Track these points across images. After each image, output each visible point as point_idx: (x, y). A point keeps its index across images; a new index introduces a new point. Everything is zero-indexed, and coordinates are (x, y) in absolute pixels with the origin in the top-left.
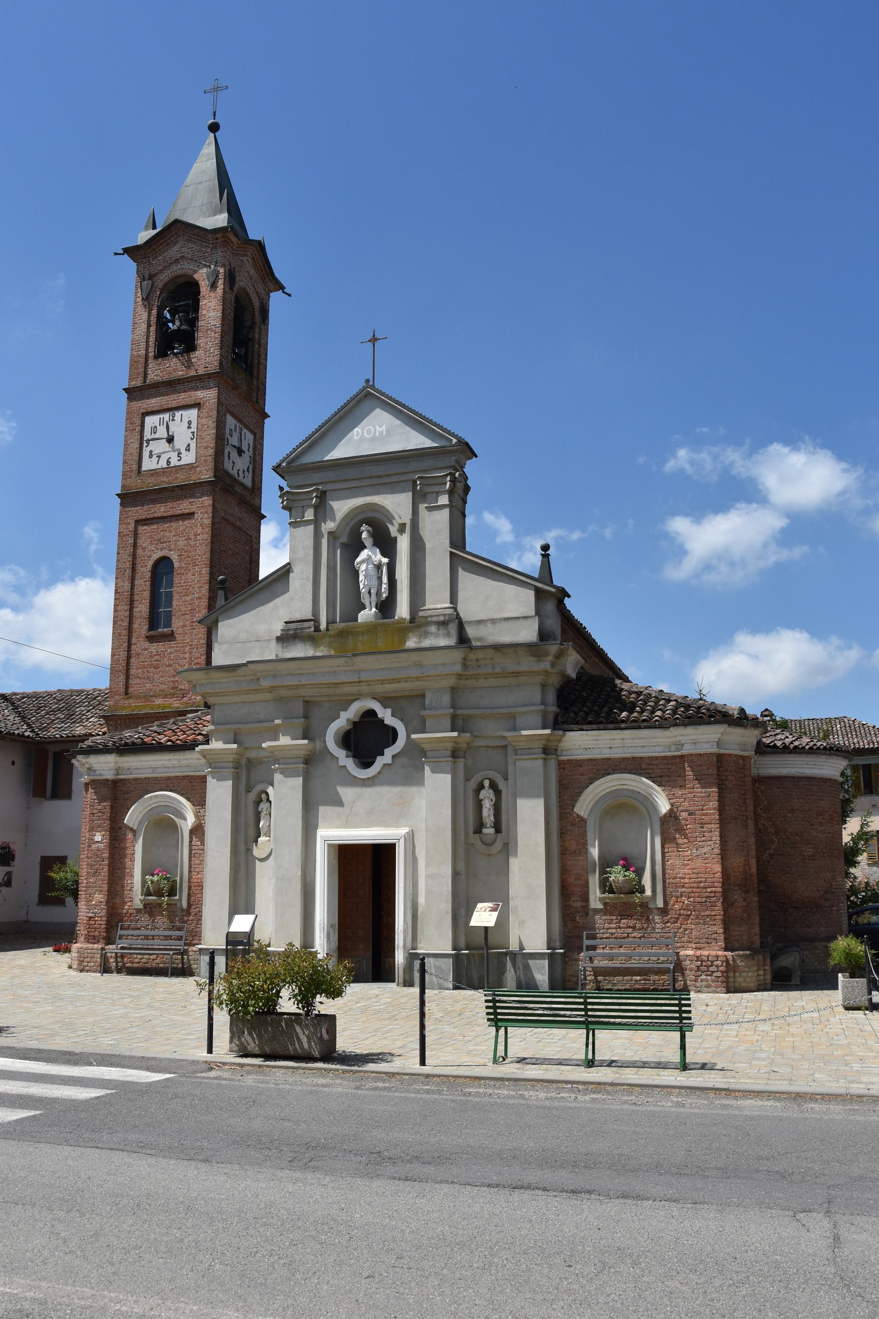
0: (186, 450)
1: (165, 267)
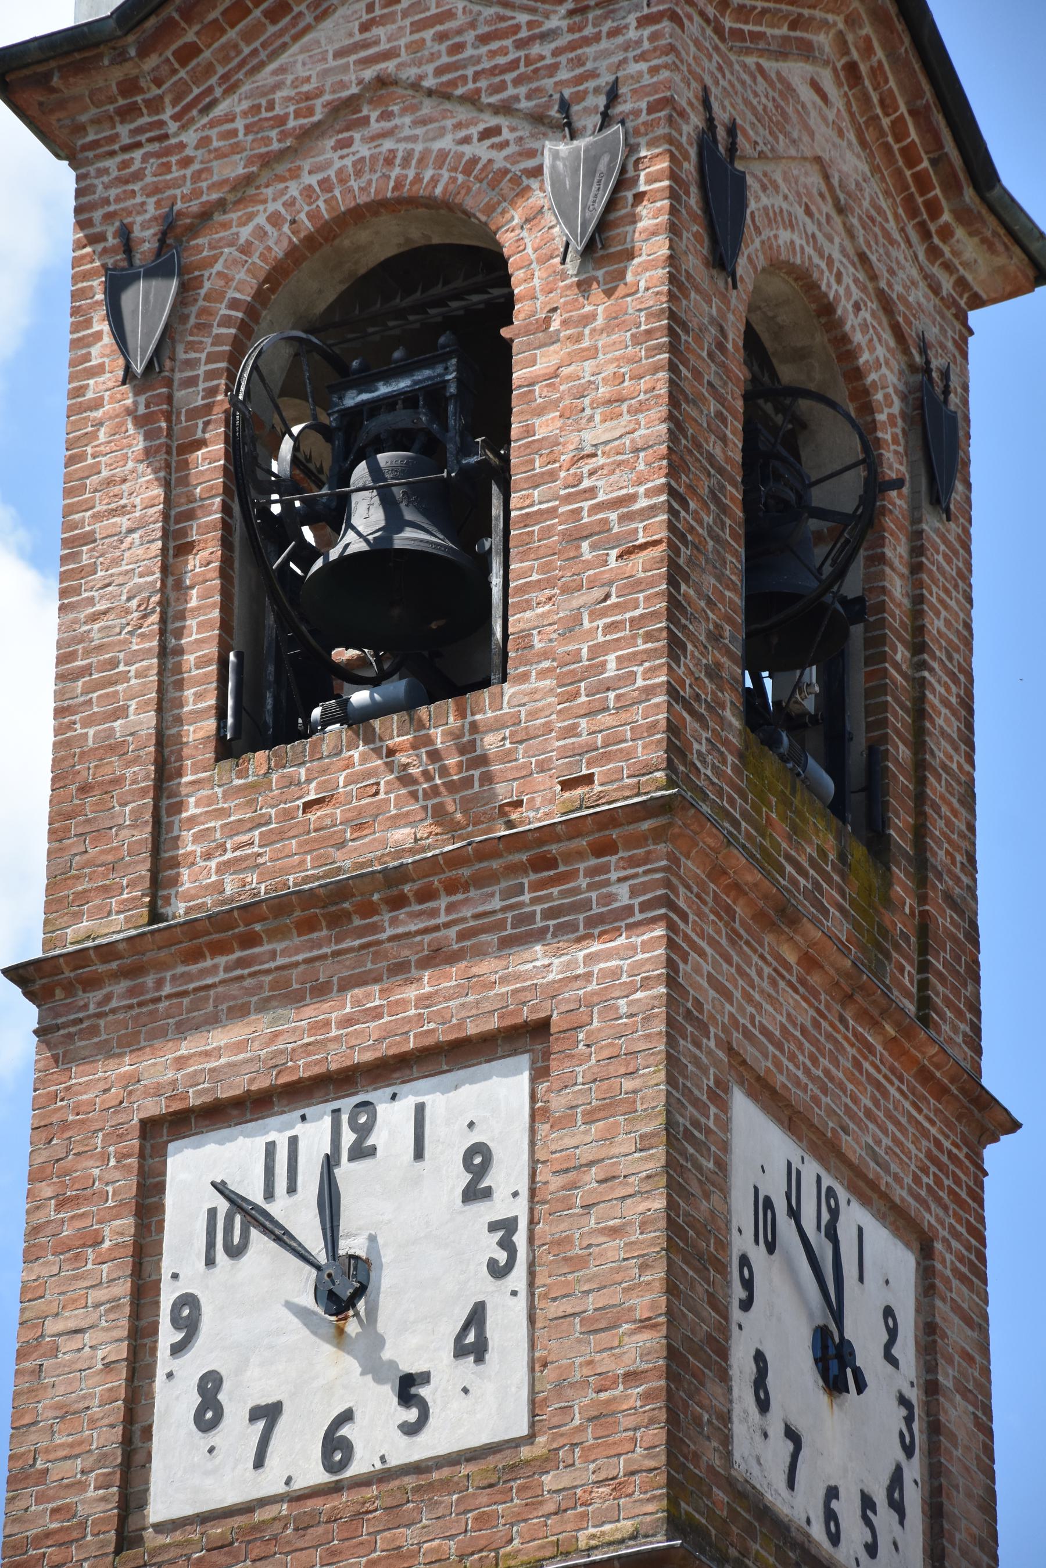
0: (461, 1351)
1: (267, 161)
